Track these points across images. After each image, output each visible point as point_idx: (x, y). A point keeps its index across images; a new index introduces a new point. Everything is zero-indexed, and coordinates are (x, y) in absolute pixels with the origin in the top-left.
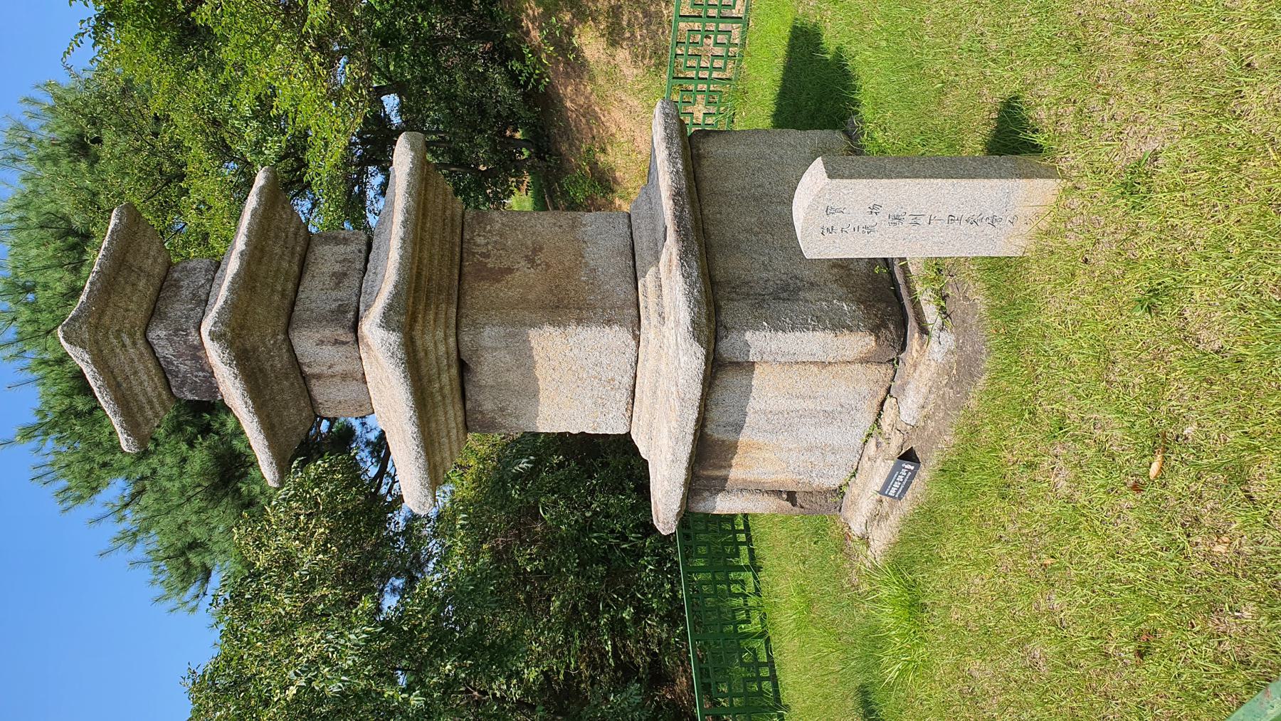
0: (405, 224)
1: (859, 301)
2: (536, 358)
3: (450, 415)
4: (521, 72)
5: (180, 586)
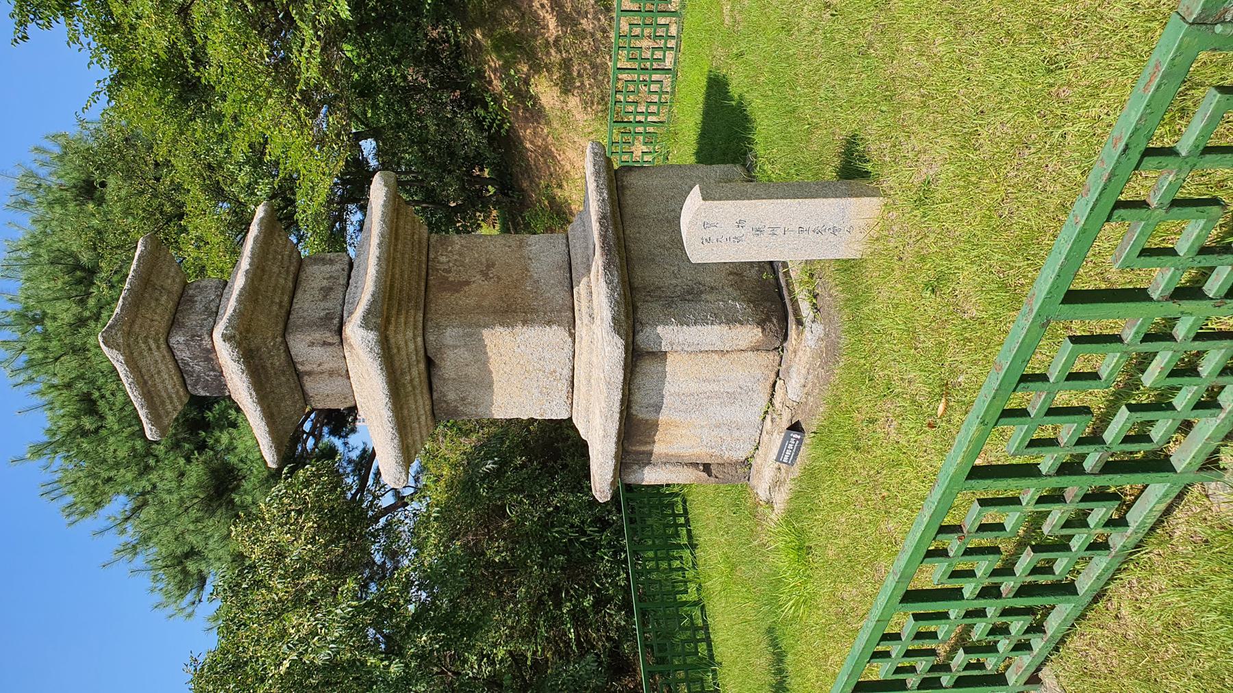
0: (380, 245)
1: (749, 301)
2: (490, 354)
3: (420, 405)
4: (484, 118)
5: (177, 593)
